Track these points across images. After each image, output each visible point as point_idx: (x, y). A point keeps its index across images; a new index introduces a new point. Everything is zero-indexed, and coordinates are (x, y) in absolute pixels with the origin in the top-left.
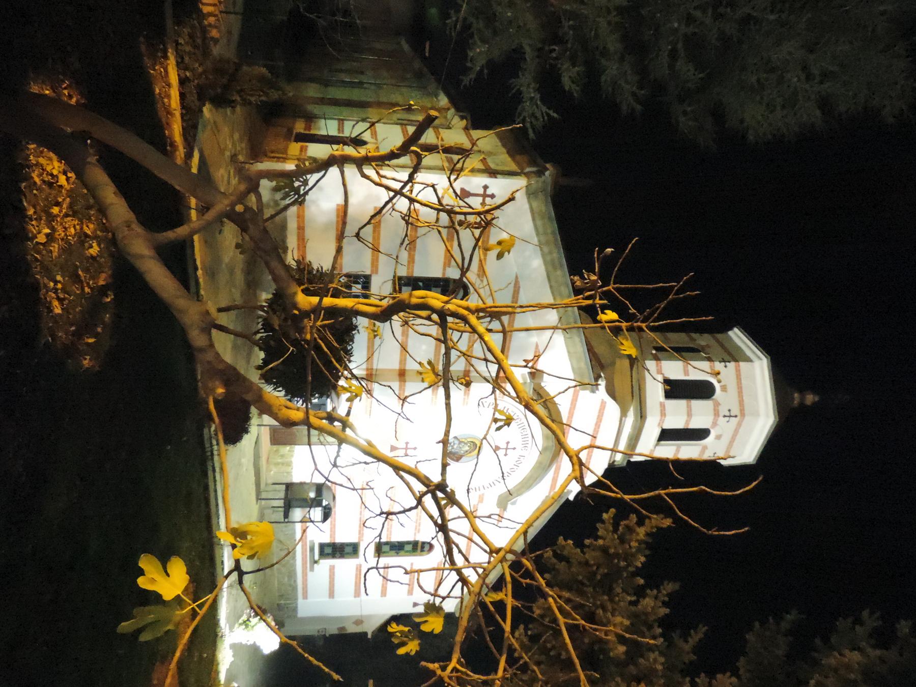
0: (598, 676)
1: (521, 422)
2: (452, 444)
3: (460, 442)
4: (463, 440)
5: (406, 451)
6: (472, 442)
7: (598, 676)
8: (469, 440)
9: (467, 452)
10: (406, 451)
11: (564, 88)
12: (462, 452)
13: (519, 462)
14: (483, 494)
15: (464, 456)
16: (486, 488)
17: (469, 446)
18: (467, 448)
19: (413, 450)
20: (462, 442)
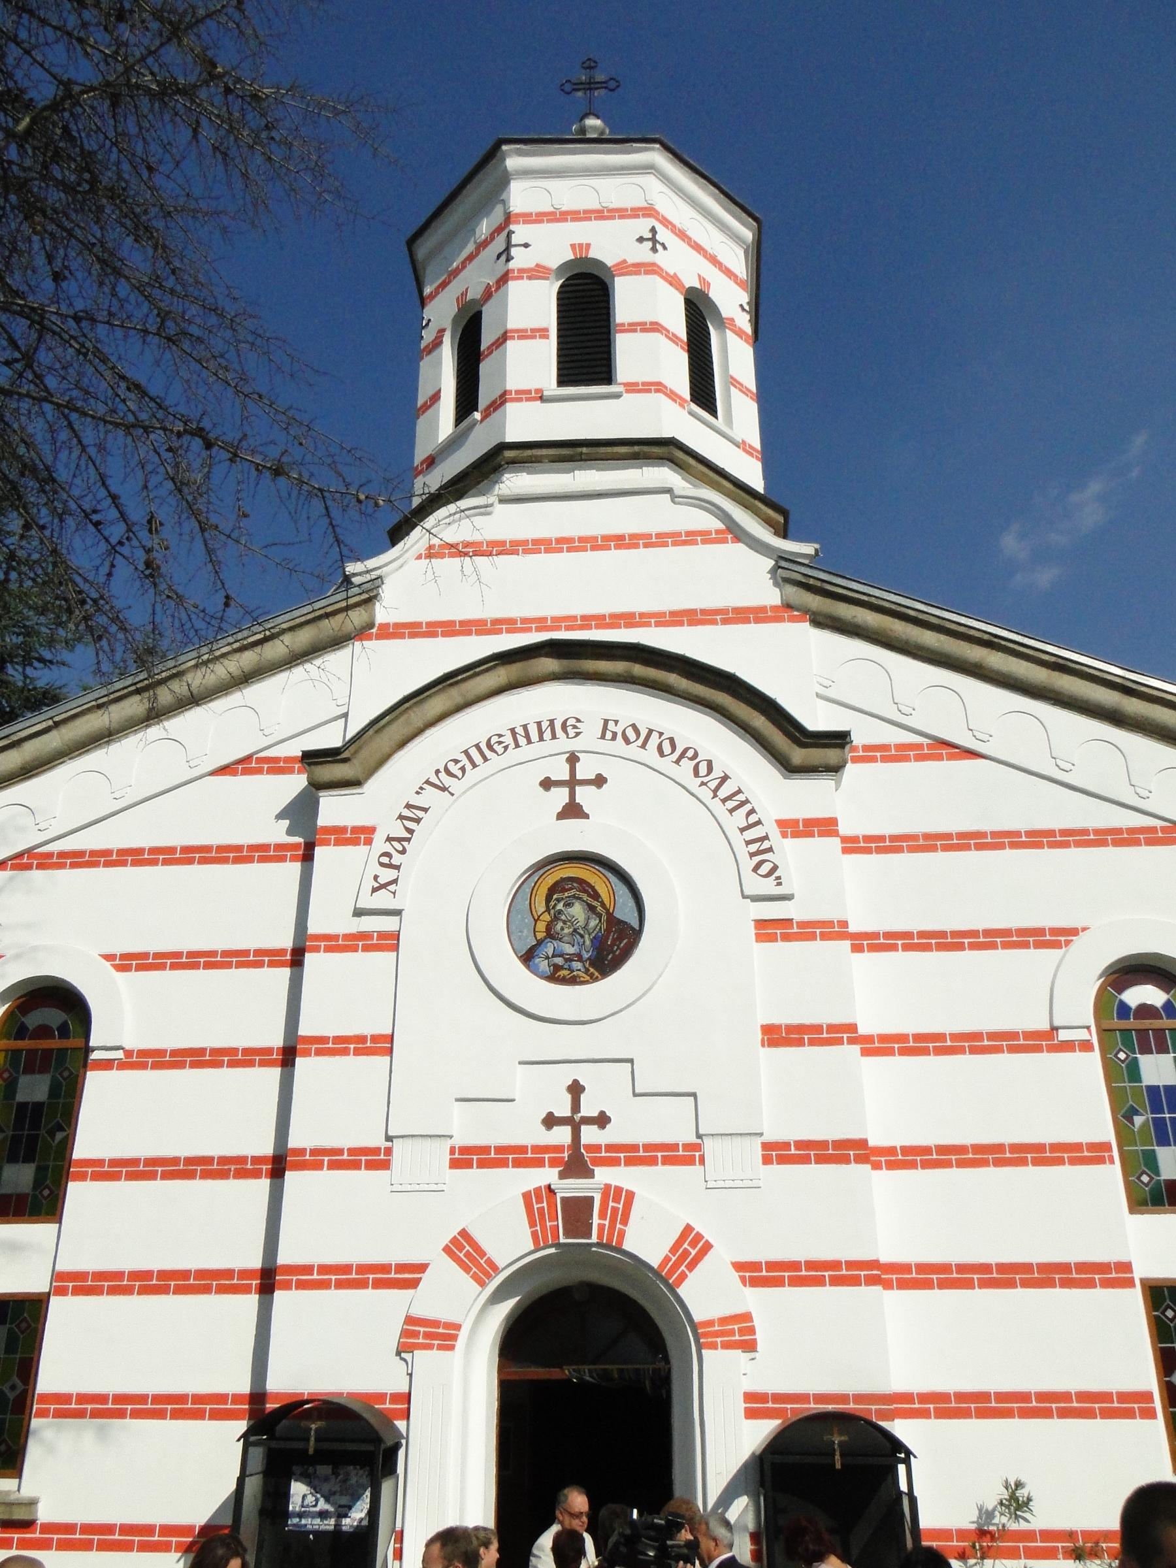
0: (838, 1466)
1: (463, 757)
2: (559, 961)
3: (550, 935)
4: (541, 926)
5: (572, 795)
6: (548, 899)
7: (838, 1466)
8: (541, 908)
9: (592, 909)
10: (572, 795)
11: (309, 1484)
12: (593, 923)
13: (631, 734)
14: (782, 824)
15: (610, 915)
16: (753, 819)
17: (568, 905)
18: (577, 911)
19: (522, 248)
20: (549, 928)
